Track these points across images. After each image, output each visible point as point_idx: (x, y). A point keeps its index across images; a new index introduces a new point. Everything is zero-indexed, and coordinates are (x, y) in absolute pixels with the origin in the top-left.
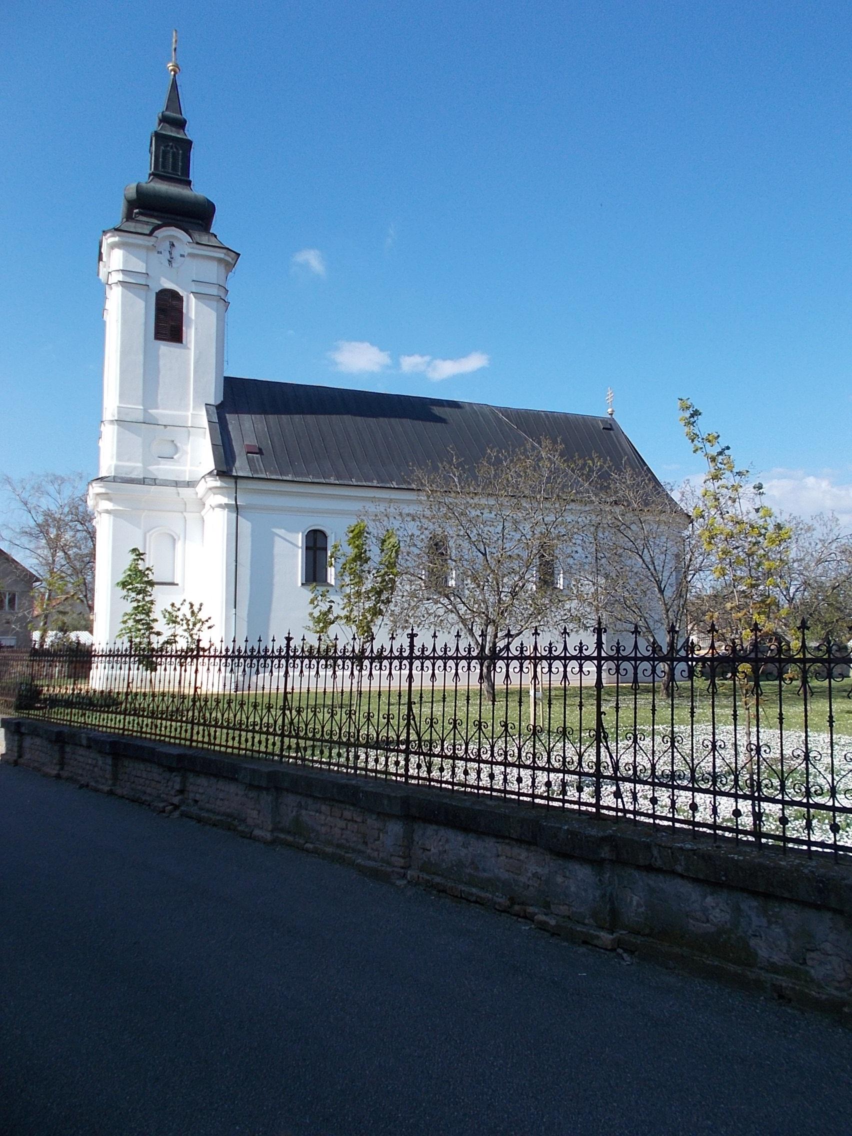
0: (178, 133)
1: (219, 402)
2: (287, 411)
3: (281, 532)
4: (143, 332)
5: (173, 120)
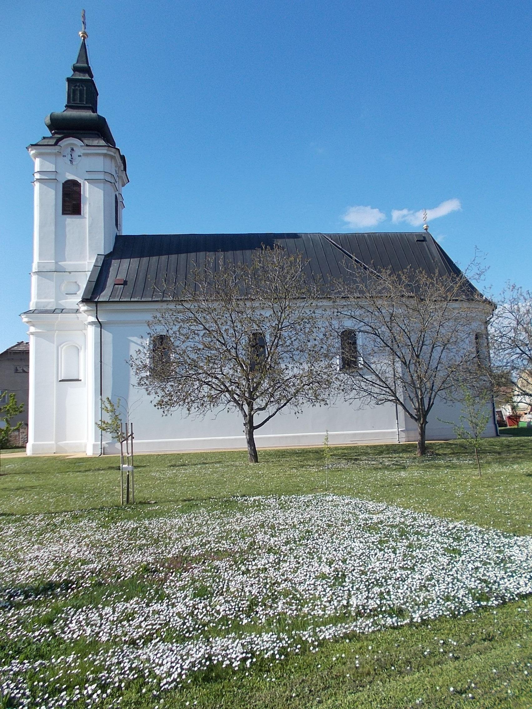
0: (84, 76)
1: (107, 253)
2: (169, 252)
3: (134, 339)
4: (54, 211)
5: (83, 68)
